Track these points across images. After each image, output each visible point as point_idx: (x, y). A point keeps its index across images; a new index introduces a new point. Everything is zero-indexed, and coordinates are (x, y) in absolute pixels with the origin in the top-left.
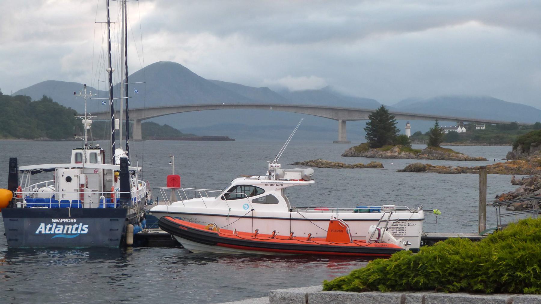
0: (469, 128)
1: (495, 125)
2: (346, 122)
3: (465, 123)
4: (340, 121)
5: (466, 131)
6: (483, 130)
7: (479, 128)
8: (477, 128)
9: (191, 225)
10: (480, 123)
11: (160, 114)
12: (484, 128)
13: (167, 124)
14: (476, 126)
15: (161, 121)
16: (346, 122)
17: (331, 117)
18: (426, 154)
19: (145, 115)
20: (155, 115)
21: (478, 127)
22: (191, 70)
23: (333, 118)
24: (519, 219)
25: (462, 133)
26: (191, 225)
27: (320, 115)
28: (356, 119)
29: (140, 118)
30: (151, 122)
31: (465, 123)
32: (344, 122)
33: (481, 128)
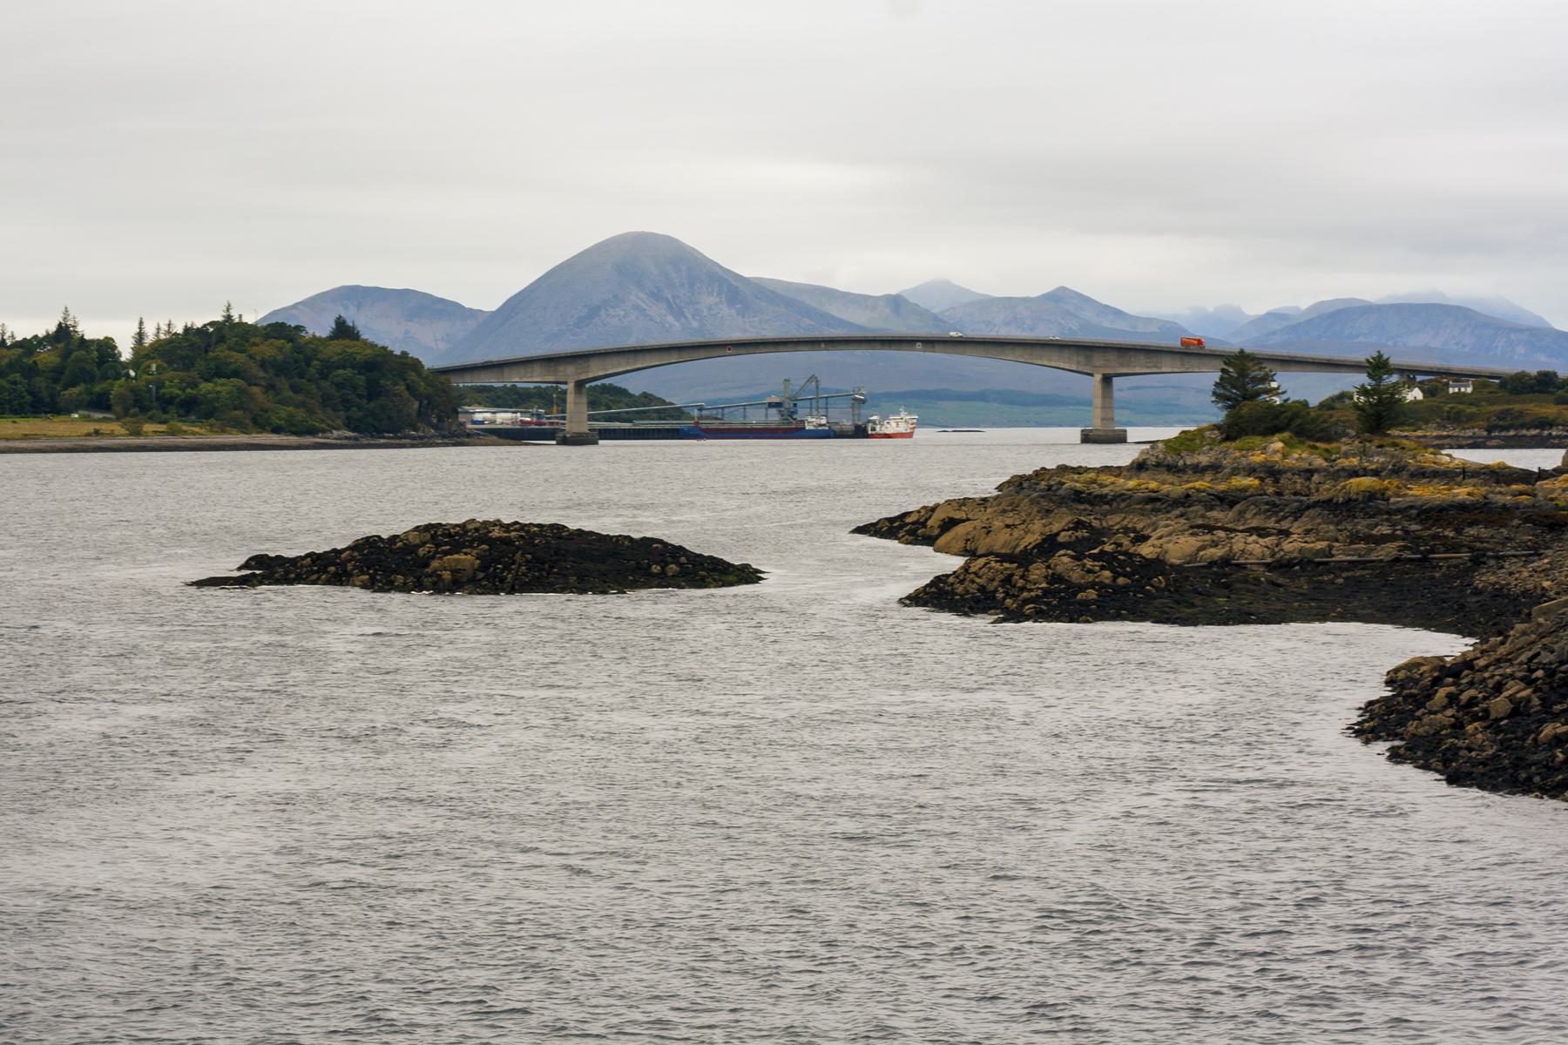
0: (1429, 392)
1: (1497, 381)
2: (1114, 379)
3: (1419, 378)
4: (1098, 377)
5: (1424, 397)
6: (1464, 394)
7: (1456, 390)
8: (1451, 390)
9: (690, 599)
10: (1459, 377)
11: (639, 366)
12: (1469, 390)
13: (650, 392)
14: (1447, 385)
15: (634, 384)
16: (1114, 379)
17: (1074, 368)
18: (1354, 455)
19: (595, 369)
20: (620, 370)
21: (1453, 387)
22: (973, 290)
23: (1080, 369)
24: (1484, 563)
25: (1415, 402)
26: (690, 599)
27: (1046, 363)
28: (1138, 370)
29: (583, 377)
30: (102, 338)
31: (1419, 378)
32: (1107, 380)
33: (1463, 390)
